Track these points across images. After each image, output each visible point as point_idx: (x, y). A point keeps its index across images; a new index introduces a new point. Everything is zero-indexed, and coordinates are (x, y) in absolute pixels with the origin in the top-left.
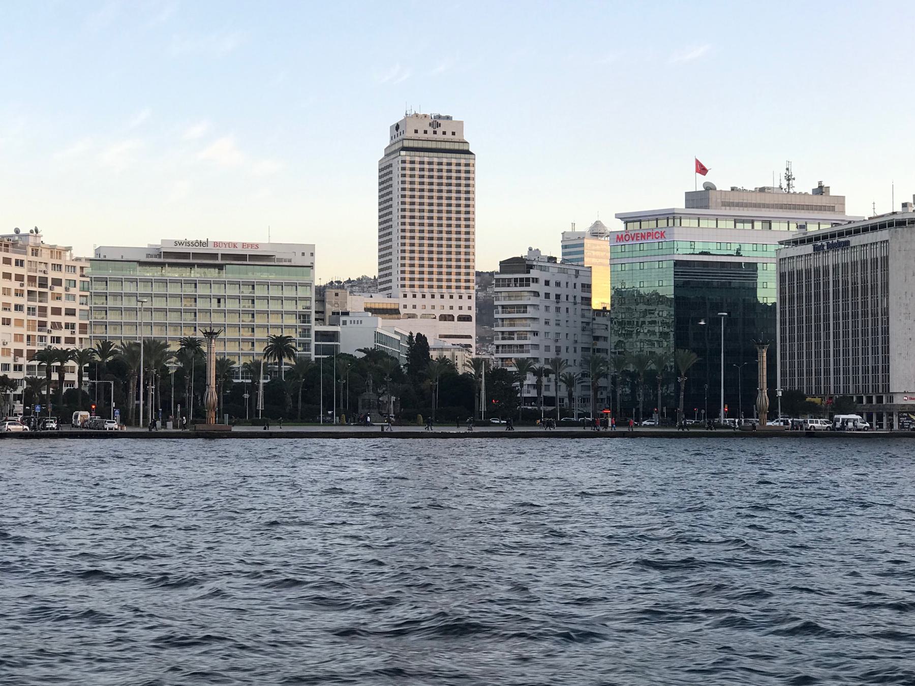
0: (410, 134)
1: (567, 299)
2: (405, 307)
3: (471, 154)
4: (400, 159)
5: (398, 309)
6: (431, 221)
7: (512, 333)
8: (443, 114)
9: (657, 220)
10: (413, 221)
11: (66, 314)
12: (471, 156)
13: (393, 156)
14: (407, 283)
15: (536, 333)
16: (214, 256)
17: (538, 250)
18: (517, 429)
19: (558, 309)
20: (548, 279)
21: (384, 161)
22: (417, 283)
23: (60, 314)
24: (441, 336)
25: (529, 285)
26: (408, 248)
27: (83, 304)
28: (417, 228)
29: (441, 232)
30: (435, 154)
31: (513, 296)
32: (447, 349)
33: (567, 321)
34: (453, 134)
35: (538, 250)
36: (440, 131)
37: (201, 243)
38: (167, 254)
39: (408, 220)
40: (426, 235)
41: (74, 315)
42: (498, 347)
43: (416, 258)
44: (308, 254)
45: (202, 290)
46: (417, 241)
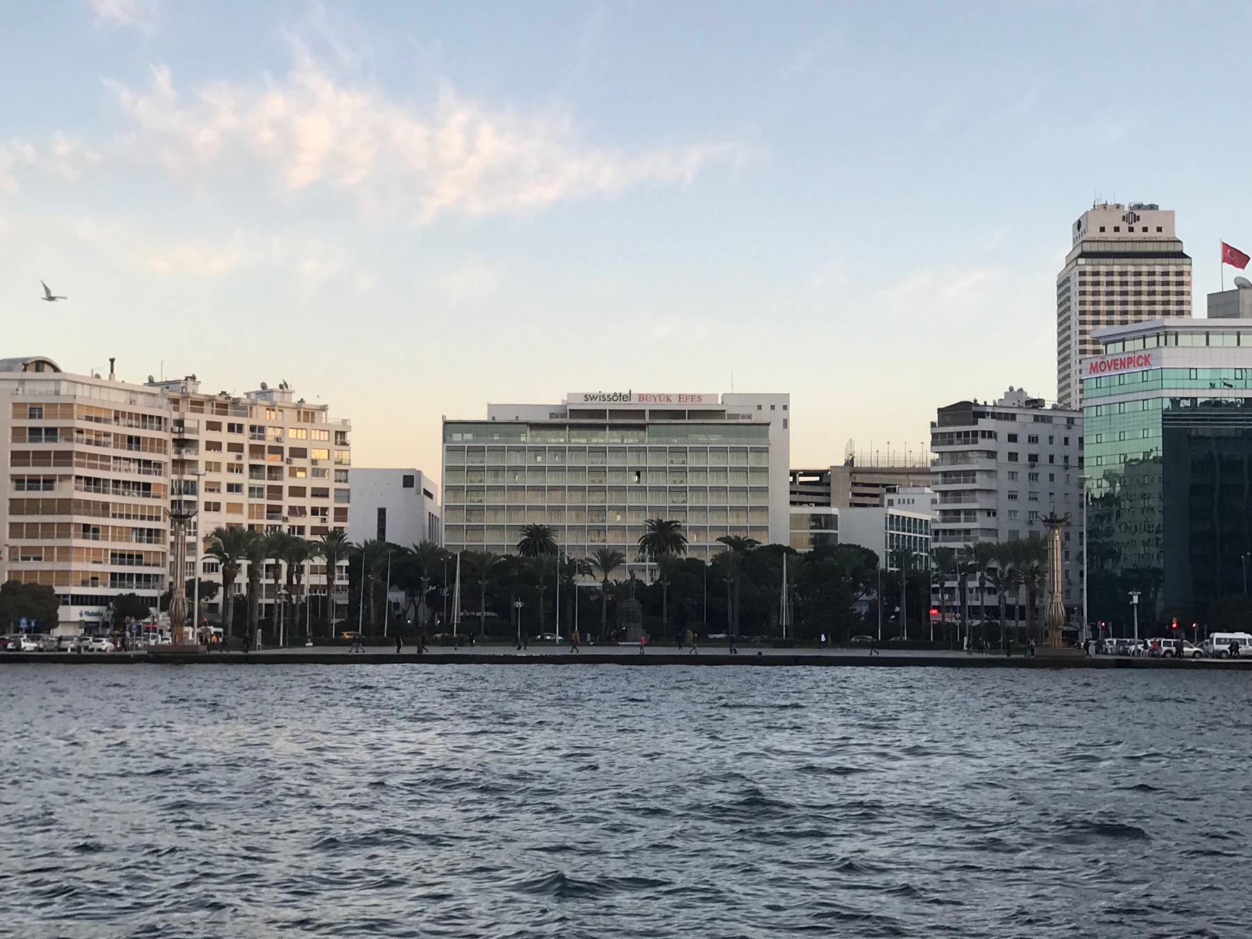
0: (1093, 233)
3: (1186, 257)
7: (957, 512)
8: (1146, 203)
9: (1207, 334)
11: (313, 495)
15: (991, 513)
16: (640, 413)
18: (743, 652)
19: (1033, 477)
23: (304, 495)
25: (976, 442)
27: (340, 481)
33: (1051, 494)
36: (1137, 226)
37: (620, 397)
38: (574, 413)
41: (327, 496)
42: (937, 532)
44: (779, 408)
45: (613, 461)
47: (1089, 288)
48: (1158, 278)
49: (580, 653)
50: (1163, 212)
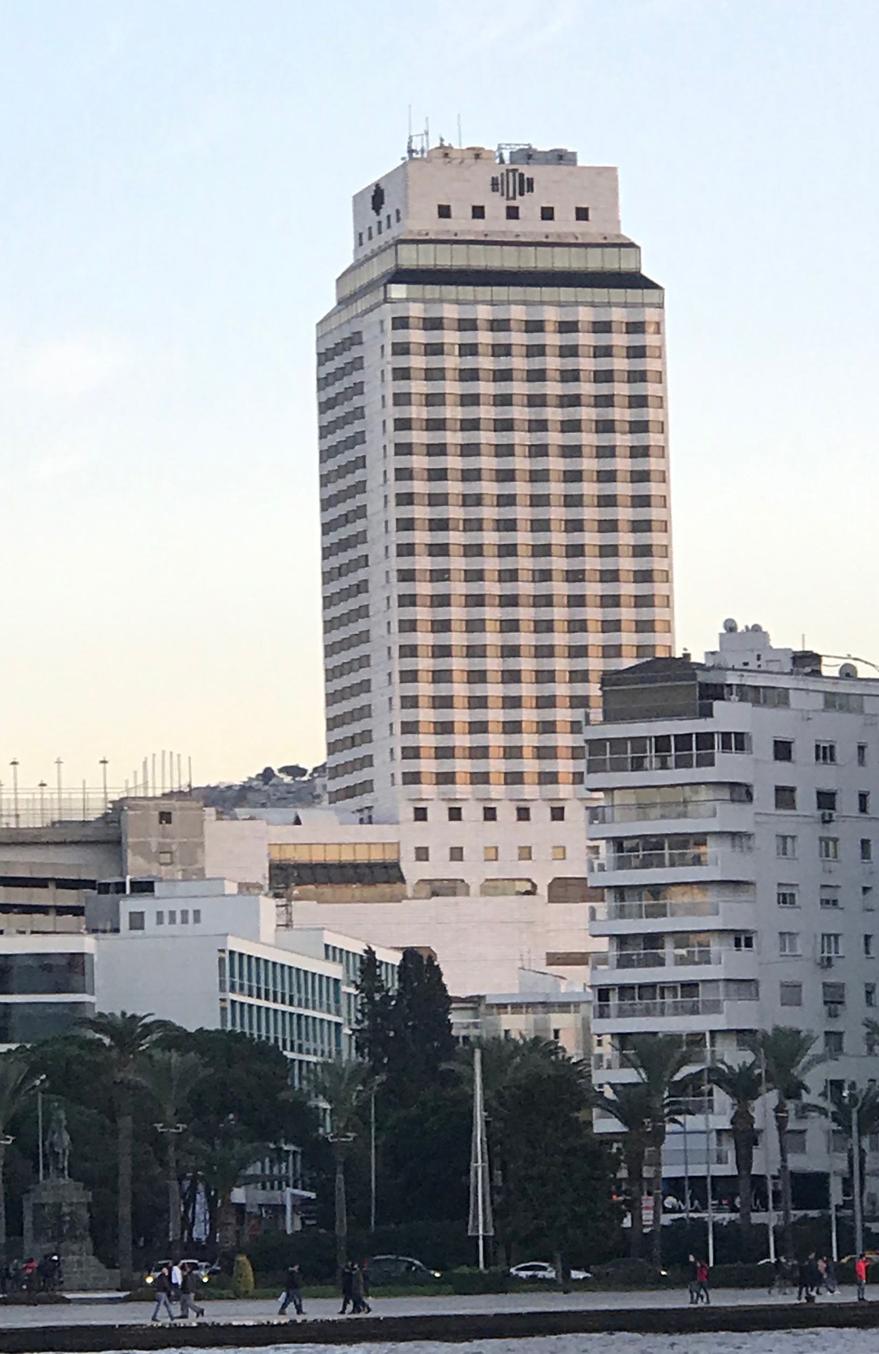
1: (863, 809)
2: (422, 854)
4: (388, 312)
5: (396, 865)
6: (508, 538)
7: (653, 940)
8: (542, 145)
10: (440, 537)
12: (649, 295)
13: (361, 305)
14: (428, 766)
17: (756, 628)
20: (784, 735)
21: (334, 323)
22: (462, 766)
24: (554, 959)
26: (424, 638)
28: (457, 563)
29: (545, 575)
30: (516, 292)
31: (653, 805)
32: (564, 1007)
33: (865, 890)
34: (582, 214)
35: (756, 628)
36: (529, 205)
39: (421, 537)
40: (492, 588)
43: (456, 676)
46: (457, 613)
47: (417, 362)
48: (518, 338)
49: (206, 1319)
50: (583, 168)
